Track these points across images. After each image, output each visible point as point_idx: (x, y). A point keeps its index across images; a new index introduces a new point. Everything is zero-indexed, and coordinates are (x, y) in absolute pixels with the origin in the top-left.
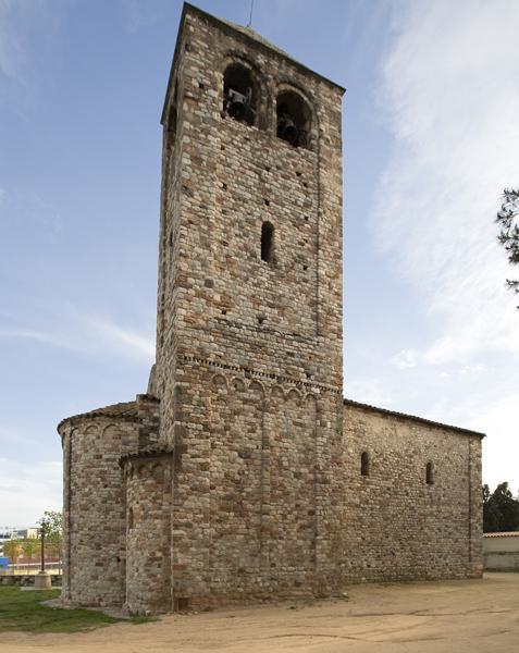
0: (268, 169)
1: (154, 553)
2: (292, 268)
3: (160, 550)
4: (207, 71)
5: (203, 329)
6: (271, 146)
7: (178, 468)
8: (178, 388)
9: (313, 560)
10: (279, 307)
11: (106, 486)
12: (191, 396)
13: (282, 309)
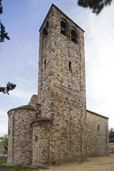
0: (70, 48)
1: (44, 149)
2: (75, 73)
3: (47, 148)
4: (55, 21)
5: (57, 87)
6: (71, 43)
7: (52, 125)
8: (52, 103)
9: (81, 150)
10: (73, 83)
11: (25, 129)
12: (55, 105)
13: (73, 83)
